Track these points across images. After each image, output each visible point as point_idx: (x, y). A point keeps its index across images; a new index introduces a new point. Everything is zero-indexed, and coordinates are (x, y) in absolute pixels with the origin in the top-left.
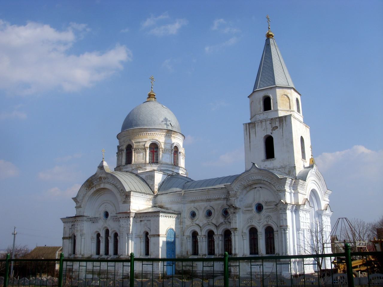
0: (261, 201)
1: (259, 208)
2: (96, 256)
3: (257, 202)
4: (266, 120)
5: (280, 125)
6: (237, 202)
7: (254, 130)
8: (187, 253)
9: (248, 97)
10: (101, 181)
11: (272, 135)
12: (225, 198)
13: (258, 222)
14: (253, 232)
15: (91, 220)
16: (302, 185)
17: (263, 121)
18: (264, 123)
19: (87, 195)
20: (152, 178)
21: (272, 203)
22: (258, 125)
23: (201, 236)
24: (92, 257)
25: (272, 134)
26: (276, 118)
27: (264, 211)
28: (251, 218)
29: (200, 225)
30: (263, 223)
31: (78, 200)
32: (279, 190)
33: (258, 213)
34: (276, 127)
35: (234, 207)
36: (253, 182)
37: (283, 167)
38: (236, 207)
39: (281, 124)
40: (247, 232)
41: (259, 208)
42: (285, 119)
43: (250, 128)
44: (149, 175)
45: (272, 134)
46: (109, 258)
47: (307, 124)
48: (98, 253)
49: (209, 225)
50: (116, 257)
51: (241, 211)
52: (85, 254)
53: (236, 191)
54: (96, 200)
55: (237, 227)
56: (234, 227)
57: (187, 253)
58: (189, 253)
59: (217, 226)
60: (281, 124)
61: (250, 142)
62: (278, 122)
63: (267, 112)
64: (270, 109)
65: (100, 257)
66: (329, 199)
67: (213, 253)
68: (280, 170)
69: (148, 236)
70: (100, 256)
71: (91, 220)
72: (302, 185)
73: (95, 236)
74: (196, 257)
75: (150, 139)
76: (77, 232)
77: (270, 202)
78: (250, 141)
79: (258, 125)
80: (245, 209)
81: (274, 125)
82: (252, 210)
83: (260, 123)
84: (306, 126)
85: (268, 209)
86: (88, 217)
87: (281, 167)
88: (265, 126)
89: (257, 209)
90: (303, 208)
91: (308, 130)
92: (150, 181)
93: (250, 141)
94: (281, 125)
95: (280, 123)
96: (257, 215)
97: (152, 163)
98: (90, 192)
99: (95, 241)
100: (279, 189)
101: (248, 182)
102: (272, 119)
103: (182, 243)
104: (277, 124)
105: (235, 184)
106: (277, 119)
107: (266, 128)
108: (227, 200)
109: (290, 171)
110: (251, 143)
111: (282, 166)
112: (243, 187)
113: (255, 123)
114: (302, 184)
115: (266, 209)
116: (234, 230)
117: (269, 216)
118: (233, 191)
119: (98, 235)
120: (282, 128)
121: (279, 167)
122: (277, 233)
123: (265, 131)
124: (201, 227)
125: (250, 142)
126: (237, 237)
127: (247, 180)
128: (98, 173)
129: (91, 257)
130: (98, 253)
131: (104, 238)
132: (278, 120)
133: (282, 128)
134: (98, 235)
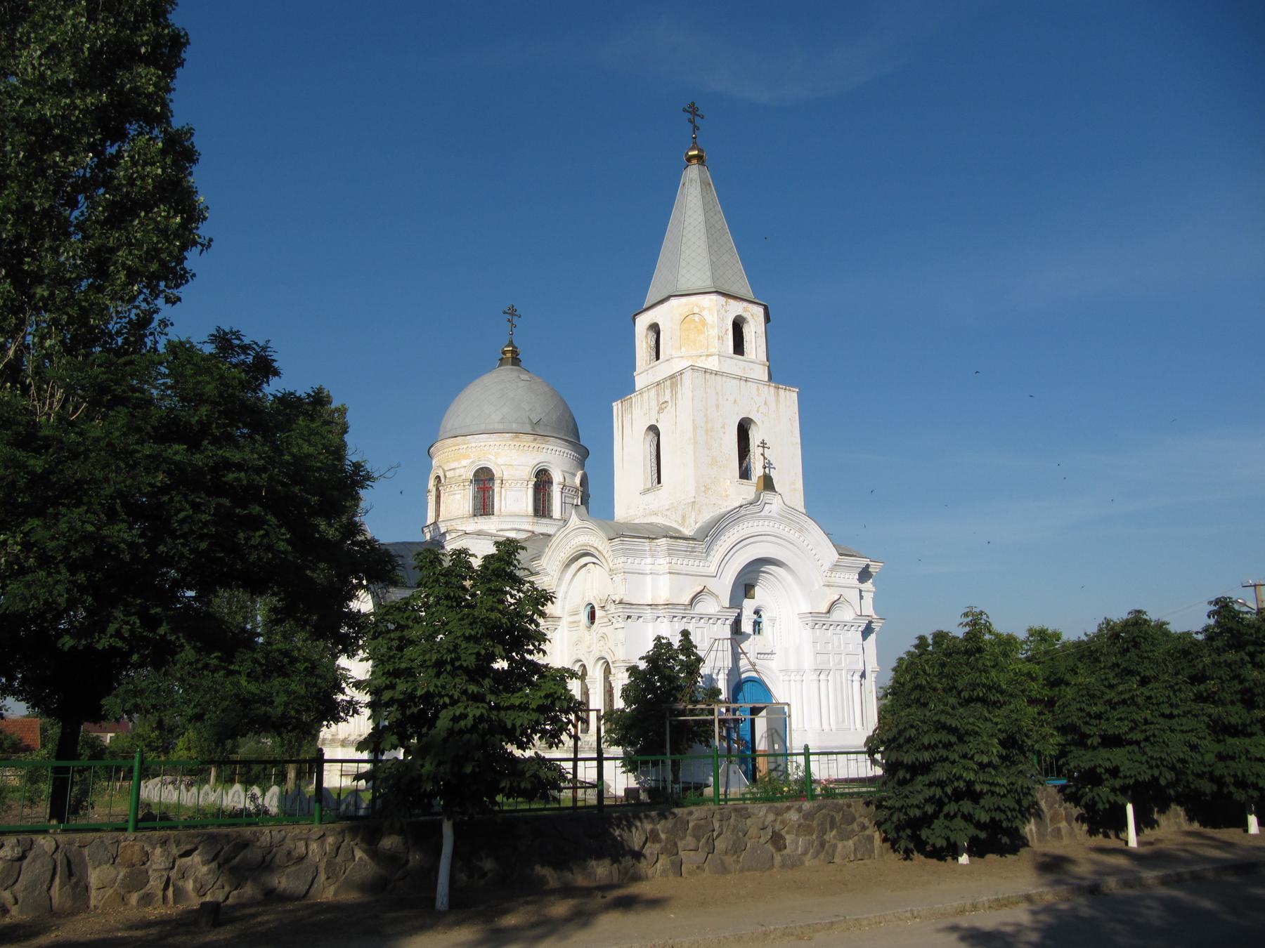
0: (594, 596)
18: (645, 395)
121: (667, 507)
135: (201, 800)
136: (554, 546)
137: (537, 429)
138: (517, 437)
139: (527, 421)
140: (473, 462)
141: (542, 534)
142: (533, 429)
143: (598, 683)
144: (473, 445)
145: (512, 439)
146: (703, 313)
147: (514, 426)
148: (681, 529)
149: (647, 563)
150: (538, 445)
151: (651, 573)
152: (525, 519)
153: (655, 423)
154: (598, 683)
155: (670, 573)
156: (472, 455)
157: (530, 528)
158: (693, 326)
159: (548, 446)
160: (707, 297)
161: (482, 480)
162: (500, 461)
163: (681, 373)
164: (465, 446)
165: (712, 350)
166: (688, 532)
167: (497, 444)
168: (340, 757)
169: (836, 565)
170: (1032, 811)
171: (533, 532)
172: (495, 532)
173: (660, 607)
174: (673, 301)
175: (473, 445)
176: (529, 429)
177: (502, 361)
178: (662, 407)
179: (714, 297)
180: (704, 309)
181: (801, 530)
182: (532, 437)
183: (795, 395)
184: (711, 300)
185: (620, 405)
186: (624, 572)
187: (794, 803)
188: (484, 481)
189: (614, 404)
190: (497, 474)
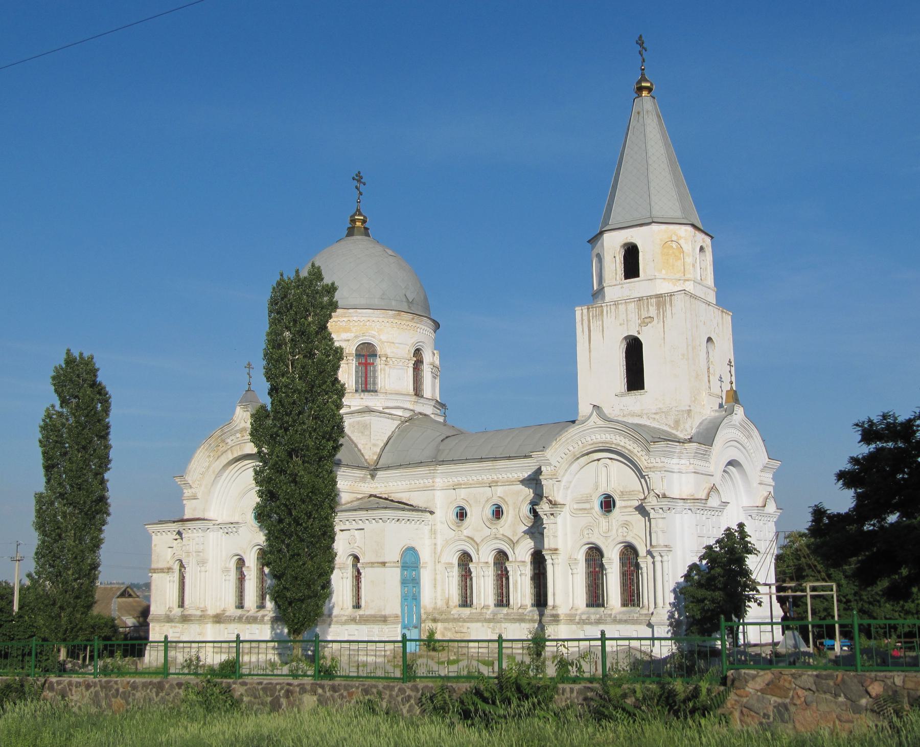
0: (613, 489)
1: (608, 504)
2: (232, 611)
3: (603, 489)
4: (627, 301)
5: (658, 314)
6: (558, 490)
7: (601, 322)
8: (447, 604)
9: (589, 242)
10: (243, 438)
11: (640, 337)
12: (533, 479)
13: (604, 535)
14: (595, 555)
15: (221, 528)
16: (702, 454)
17: (621, 303)
18: (622, 308)
19: (211, 469)
20: (364, 429)
21: (635, 495)
22: (609, 311)
23: (478, 563)
24: (226, 614)
25: (639, 333)
26: (651, 297)
27: (616, 512)
28: (590, 528)
29: (475, 539)
30: (614, 539)
31: (190, 482)
32: (650, 468)
33: (604, 514)
34: (650, 317)
35: (550, 501)
36: (593, 446)
37: (663, 412)
38: (555, 501)
39: (661, 310)
40: (581, 556)
41: (608, 504)
42: (671, 300)
43: (591, 318)
44: (358, 423)
45: (639, 333)
46: (266, 615)
47: (724, 308)
48: (240, 606)
49: (497, 538)
50: (239, 612)
51: (566, 510)
52: (209, 608)
53: (557, 464)
54: (231, 481)
55: (559, 547)
56: (553, 546)
57: (447, 604)
58: (451, 603)
59: (515, 542)
60: (661, 310)
61: (590, 352)
62: (655, 307)
63: (631, 282)
64: (637, 275)
65: (244, 615)
66: (773, 479)
67: (505, 602)
68: (657, 417)
69: (359, 565)
70: (244, 613)
71: (221, 528)
72: (702, 454)
73: (232, 565)
74: (466, 611)
75: (358, 334)
76: (188, 556)
77: (630, 493)
78: (590, 348)
79: (609, 311)
80: (576, 506)
81: (644, 314)
82: (592, 508)
83: (613, 308)
84: (722, 312)
85: (625, 507)
86: (214, 522)
87: (658, 411)
88: (625, 315)
89: (602, 508)
90: (703, 505)
91: (728, 319)
92: (360, 434)
93: (590, 348)
94: (661, 313)
95: (658, 309)
96: (603, 521)
97: (363, 391)
98: (217, 462)
99: (233, 575)
100: (650, 465)
101: (583, 447)
102: (640, 299)
103: (435, 579)
104: (653, 311)
105: (553, 451)
106: (652, 300)
107: (627, 321)
108: (536, 484)
109: (679, 420)
110: (592, 353)
111: (660, 408)
112: (570, 458)
113: (602, 306)
114: (702, 452)
115: (620, 508)
116: (551, 552)
117: (625, 522)
118: (550, 464)
119: (241, 562)
120: (664, 322)
121: (654, 411)
122: (646, 560)
123: (625, 326)
124: (477, 545)
125: (590, 352)
126: (559, 569)
127: (580, 443)
128: (238, 421)
129: (224, 614)
130: (240, 606)
131: (253, 569)
132: (654, 301)
133: (664, 322)
134: (241, 562)
135: (173, 676)
136: (563, 439)
137: (412, 308)
138: (399, 315)
139: (404, 299)
140: (356, 337)
141: (421, 414)
142: (409, 308)
143: (232, 572)
144: (355, 318)
145: (394, 317)
146: (680, 242)
147: (394, 303)
148: (674, 432)
149: (674, 463)
150: (415, 325)
151: (679, 472)
152: (408, 398)
153: (636, 334)
154: (232, 572)
155: (695, 472)
156: (354, 330)
157: (411, 408)
158: (671, 252)
159: (421, 326)
160: (684, 228)
161: (363, 356)
162: (384, 338)
163: (671, 295)
164: (346, 319)
165: (688, 276)
166: (681, 435)
167: (381, 320)
168: (198, 640)
169: (765, 467)
170: (840, 696)
171: (413, 411)
172: (381, 409)
173: (689, 501)
174: (654, 227)
175: (355, 318)
176: (405, 307)
177: (351, 232)
178: (646, 321)
179: (689, 228)
180: (681, 237)
181: (749, 437)
182: (411, 316)
183: (730, 318)
184: (686, 231)
185: (585, 311)
186: (665, 471)
187: (762, 673)
188: (366, 356)
189: (576, 309)
190: (379, 351)
